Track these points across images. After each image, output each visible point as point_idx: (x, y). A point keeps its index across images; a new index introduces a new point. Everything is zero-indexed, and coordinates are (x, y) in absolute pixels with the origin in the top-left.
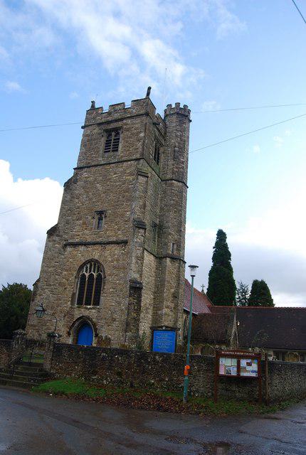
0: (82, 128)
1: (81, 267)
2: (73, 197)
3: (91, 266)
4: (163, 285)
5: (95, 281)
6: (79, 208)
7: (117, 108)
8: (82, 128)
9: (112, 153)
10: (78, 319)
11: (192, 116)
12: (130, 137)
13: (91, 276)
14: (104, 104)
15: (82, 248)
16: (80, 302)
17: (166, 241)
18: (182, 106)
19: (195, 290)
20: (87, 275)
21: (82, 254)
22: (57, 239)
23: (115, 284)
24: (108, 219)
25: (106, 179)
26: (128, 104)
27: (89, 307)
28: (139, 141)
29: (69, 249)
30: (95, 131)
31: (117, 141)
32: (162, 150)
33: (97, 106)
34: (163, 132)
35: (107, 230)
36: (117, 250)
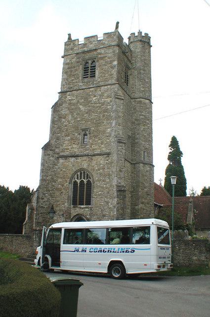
0: (63, 57)
1: (72, 177)
2: (61, 118)
3: (81, 173)
4: (138, 186)
5: (85, 186)
6: (66, 126)
7: (92, 39)
8: (63, 57)
9: (89, 79)
10: (75, 216)
11: (176, 137)
12: (105, 65)
13: (82, 182)
14: (80, 36)
15: (72, 159)
16: (75, 203)
17: (139, 150)
18: (143, 35)
19: (155, 184)
20: (79, 181)
21: (71, 165)
22: (51, 152)
23: (103, 188)
24: (92, 135)
25: (87, 102)
26: (101, 37)
27: (82, 206)
28: (113, 67)
29: (61, 161)
30: (74, 60)
31: (93, 68)
32: (129, 73)
33: (73, 38)
34: (130, 58)
35: (92, 144)
36: (101, 160)
